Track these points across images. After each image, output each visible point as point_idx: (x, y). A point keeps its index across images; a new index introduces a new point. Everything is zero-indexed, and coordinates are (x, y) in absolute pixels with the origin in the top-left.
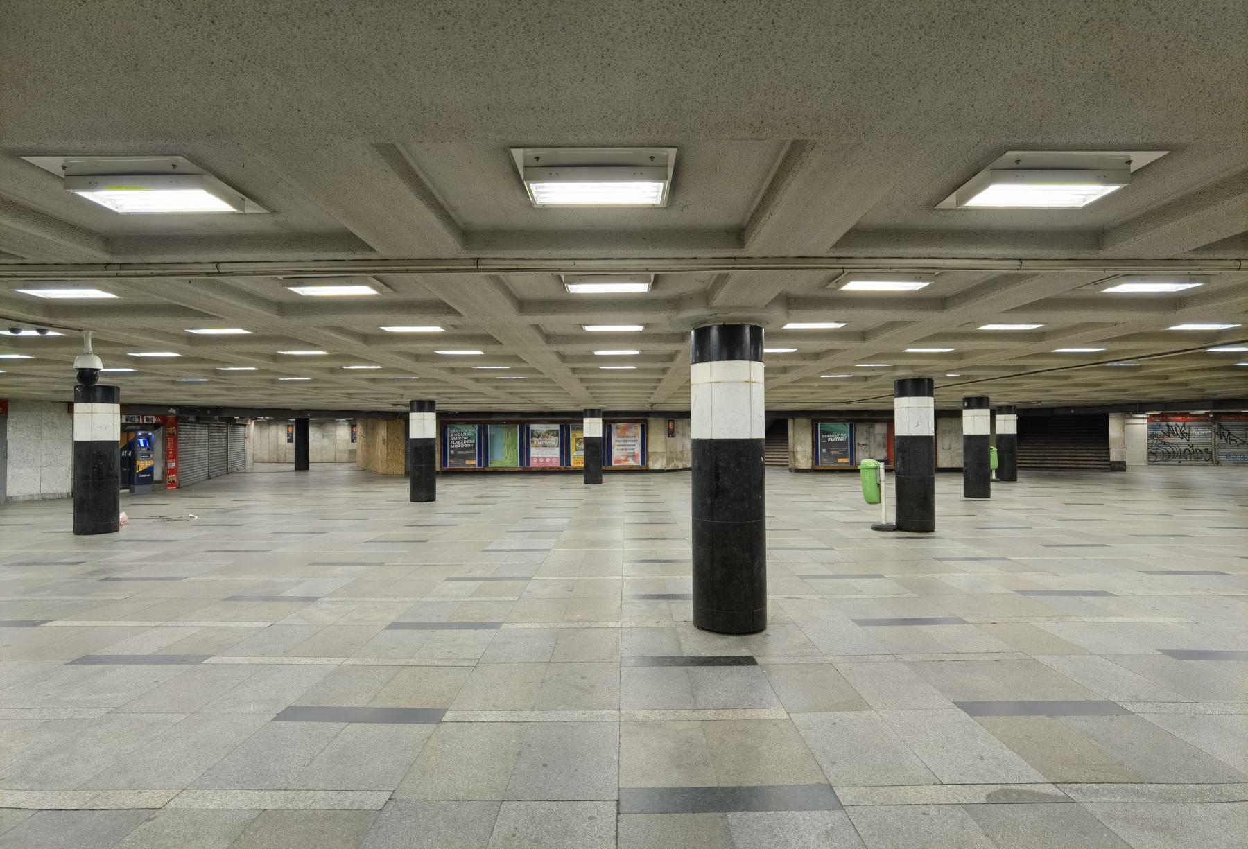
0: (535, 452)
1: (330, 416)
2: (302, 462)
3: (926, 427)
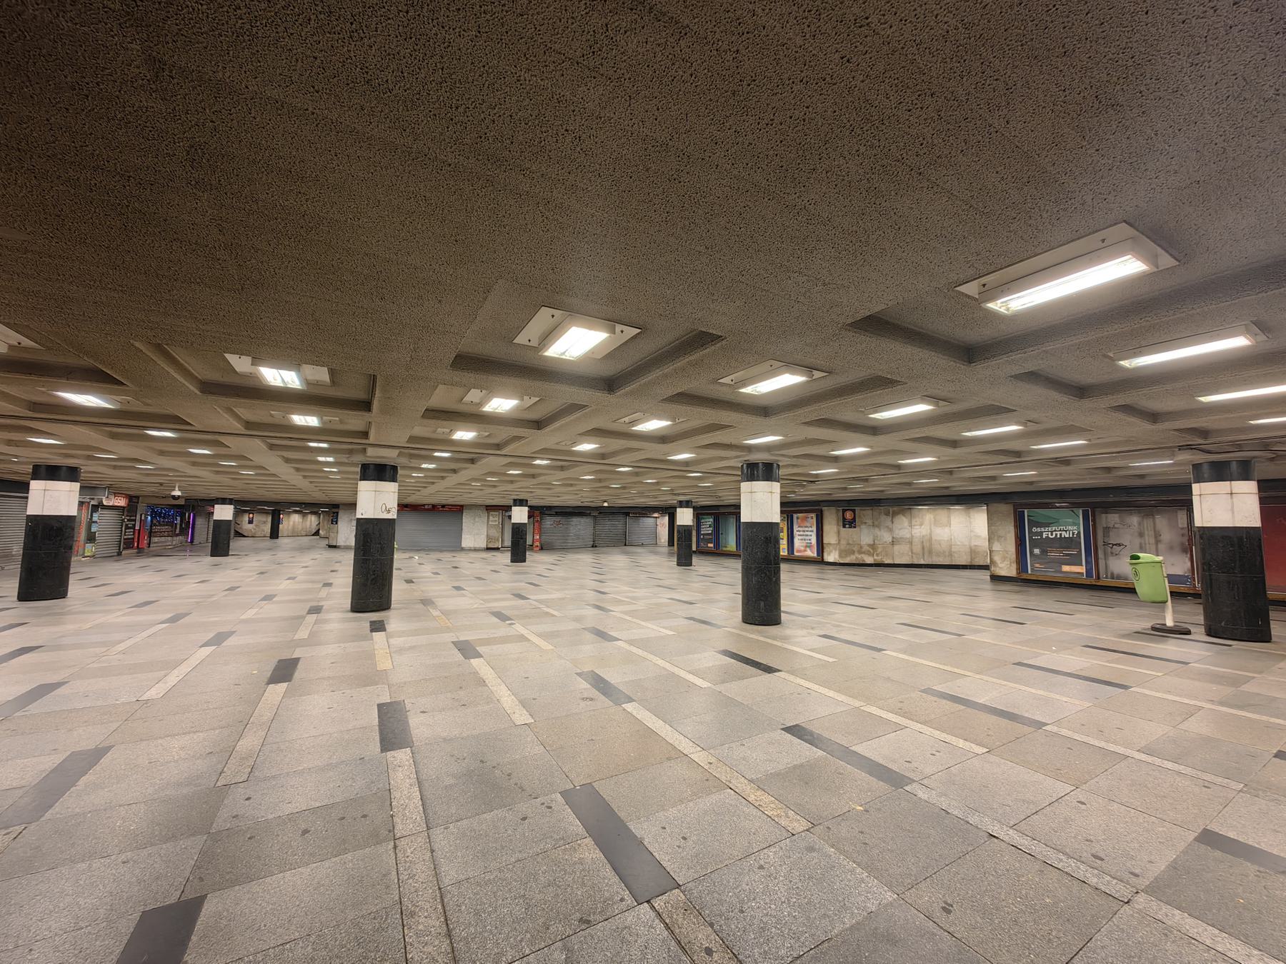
0: (798, 543)
2: (275, 534)
3: (771, 513)
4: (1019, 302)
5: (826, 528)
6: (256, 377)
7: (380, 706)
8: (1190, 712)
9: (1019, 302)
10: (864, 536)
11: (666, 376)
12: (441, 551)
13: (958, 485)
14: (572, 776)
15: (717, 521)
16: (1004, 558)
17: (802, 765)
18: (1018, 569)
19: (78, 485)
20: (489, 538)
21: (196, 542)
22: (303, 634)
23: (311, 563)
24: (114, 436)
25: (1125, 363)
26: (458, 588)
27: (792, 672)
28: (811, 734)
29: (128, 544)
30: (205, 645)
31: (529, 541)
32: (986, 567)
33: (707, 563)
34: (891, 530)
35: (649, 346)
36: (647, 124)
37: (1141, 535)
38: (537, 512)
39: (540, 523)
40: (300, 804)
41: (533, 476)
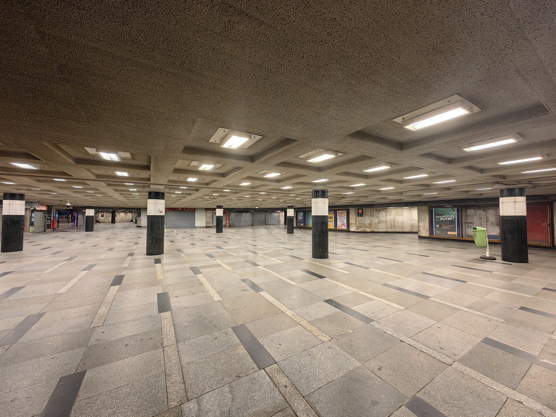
0: (339, 223)
4: (418, 126)
5: (351, 217)
6: (99, 156)
7: (158, 294)
8: (489, 292)
9: (418, 126)
10: (366, 220)
11: (275, 156)
12: (186, 228)
13: (405, 198)
14: (237, 321)
15: (305, 214)
16: (424, 229)
17: (330, 315)
18: (430, 233)
19: (24, 202)
20: (207, 222)
21: (79, 225)
22: (126, 265)
23: (129, 234)
24: (38, 181)
25: (466, 150)
26: (193, 244)
27: (330, 278)
28: (336, 302)
29: (49, 227)
30: (84, 270)
31: (224, 223)
32: (417, 233)
34: (378, 218)
35: (266, 144)
36: (252, 58)
37: (480, 219)
38: (227, 211)
39: (229, 216)
40: (125, 334)
41: (224, 196)
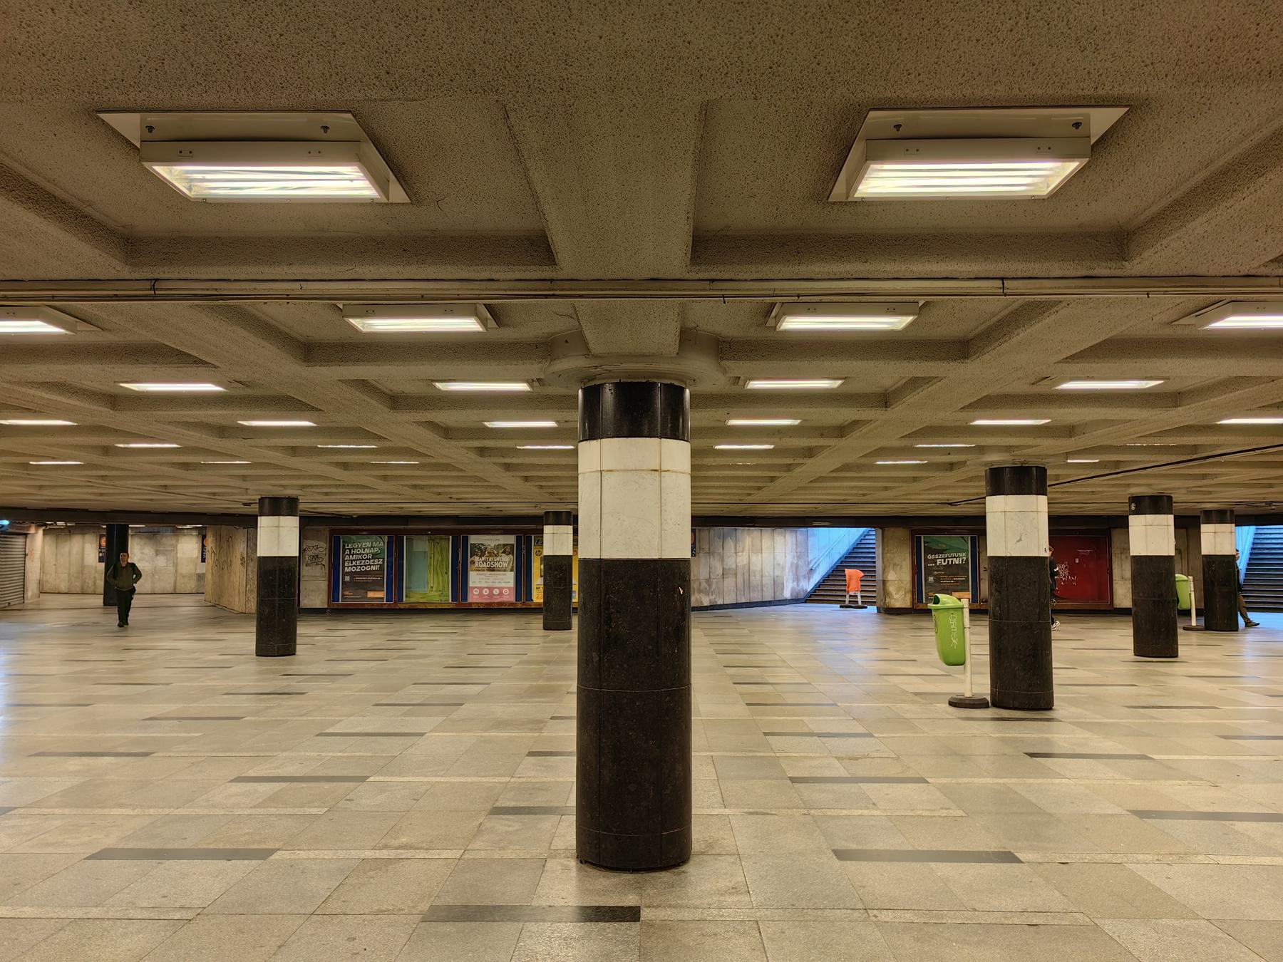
1: (164, 521)
3: (290, 525)
33: (349, 625)
